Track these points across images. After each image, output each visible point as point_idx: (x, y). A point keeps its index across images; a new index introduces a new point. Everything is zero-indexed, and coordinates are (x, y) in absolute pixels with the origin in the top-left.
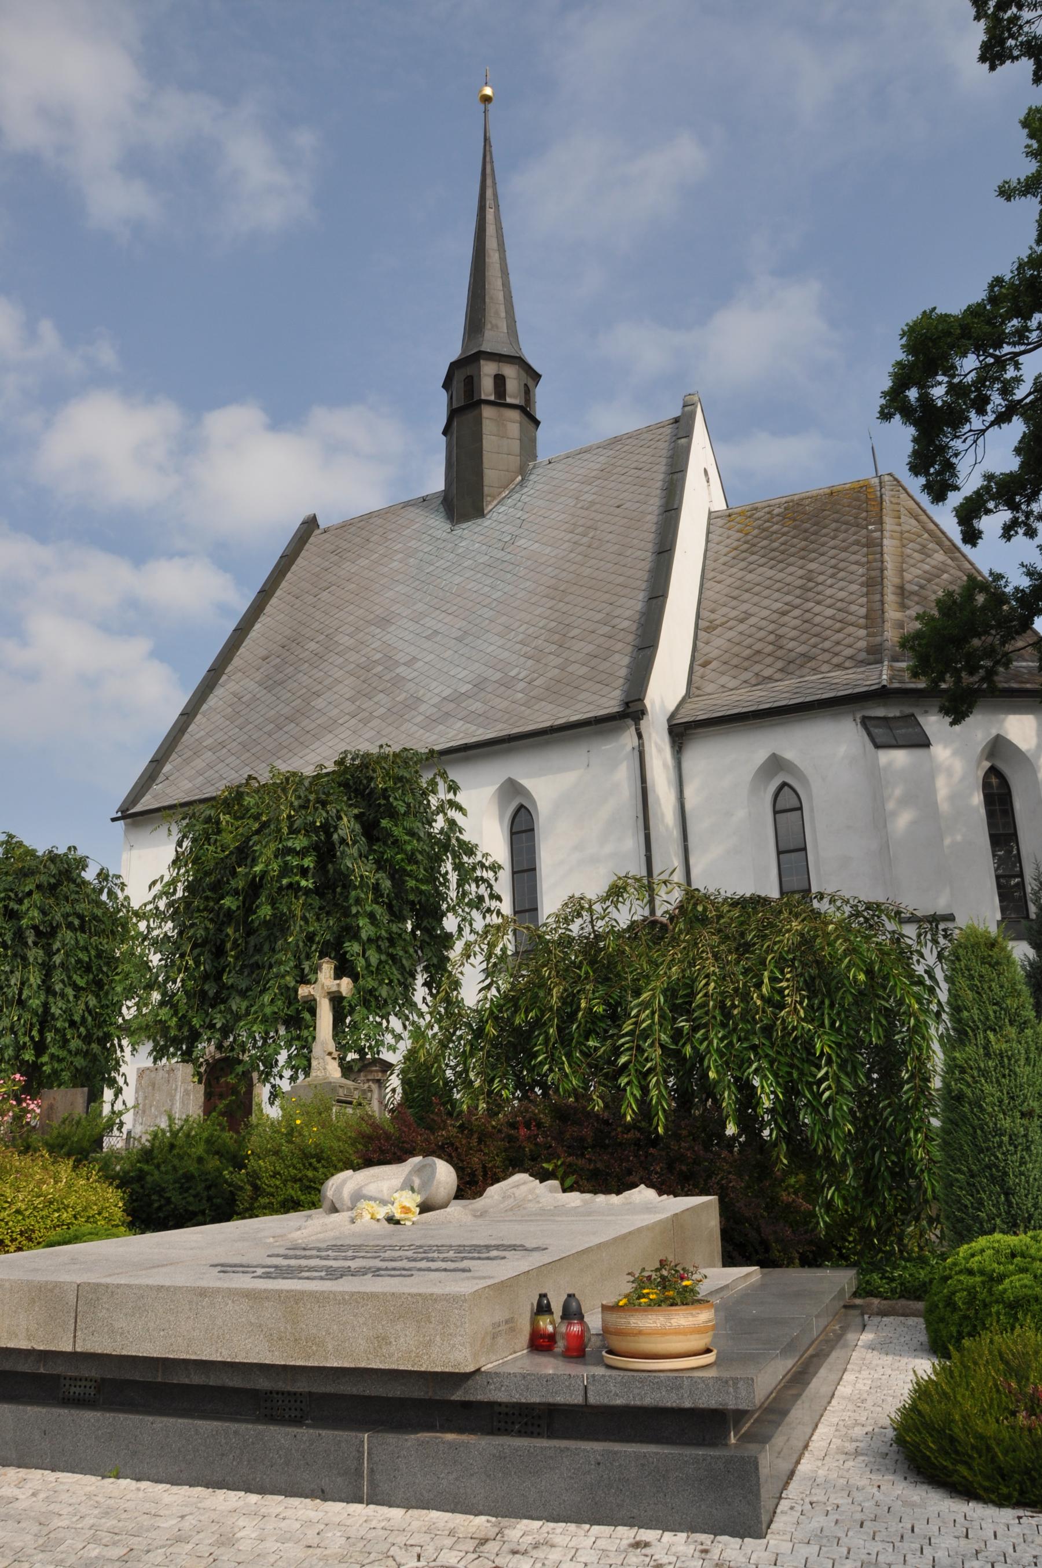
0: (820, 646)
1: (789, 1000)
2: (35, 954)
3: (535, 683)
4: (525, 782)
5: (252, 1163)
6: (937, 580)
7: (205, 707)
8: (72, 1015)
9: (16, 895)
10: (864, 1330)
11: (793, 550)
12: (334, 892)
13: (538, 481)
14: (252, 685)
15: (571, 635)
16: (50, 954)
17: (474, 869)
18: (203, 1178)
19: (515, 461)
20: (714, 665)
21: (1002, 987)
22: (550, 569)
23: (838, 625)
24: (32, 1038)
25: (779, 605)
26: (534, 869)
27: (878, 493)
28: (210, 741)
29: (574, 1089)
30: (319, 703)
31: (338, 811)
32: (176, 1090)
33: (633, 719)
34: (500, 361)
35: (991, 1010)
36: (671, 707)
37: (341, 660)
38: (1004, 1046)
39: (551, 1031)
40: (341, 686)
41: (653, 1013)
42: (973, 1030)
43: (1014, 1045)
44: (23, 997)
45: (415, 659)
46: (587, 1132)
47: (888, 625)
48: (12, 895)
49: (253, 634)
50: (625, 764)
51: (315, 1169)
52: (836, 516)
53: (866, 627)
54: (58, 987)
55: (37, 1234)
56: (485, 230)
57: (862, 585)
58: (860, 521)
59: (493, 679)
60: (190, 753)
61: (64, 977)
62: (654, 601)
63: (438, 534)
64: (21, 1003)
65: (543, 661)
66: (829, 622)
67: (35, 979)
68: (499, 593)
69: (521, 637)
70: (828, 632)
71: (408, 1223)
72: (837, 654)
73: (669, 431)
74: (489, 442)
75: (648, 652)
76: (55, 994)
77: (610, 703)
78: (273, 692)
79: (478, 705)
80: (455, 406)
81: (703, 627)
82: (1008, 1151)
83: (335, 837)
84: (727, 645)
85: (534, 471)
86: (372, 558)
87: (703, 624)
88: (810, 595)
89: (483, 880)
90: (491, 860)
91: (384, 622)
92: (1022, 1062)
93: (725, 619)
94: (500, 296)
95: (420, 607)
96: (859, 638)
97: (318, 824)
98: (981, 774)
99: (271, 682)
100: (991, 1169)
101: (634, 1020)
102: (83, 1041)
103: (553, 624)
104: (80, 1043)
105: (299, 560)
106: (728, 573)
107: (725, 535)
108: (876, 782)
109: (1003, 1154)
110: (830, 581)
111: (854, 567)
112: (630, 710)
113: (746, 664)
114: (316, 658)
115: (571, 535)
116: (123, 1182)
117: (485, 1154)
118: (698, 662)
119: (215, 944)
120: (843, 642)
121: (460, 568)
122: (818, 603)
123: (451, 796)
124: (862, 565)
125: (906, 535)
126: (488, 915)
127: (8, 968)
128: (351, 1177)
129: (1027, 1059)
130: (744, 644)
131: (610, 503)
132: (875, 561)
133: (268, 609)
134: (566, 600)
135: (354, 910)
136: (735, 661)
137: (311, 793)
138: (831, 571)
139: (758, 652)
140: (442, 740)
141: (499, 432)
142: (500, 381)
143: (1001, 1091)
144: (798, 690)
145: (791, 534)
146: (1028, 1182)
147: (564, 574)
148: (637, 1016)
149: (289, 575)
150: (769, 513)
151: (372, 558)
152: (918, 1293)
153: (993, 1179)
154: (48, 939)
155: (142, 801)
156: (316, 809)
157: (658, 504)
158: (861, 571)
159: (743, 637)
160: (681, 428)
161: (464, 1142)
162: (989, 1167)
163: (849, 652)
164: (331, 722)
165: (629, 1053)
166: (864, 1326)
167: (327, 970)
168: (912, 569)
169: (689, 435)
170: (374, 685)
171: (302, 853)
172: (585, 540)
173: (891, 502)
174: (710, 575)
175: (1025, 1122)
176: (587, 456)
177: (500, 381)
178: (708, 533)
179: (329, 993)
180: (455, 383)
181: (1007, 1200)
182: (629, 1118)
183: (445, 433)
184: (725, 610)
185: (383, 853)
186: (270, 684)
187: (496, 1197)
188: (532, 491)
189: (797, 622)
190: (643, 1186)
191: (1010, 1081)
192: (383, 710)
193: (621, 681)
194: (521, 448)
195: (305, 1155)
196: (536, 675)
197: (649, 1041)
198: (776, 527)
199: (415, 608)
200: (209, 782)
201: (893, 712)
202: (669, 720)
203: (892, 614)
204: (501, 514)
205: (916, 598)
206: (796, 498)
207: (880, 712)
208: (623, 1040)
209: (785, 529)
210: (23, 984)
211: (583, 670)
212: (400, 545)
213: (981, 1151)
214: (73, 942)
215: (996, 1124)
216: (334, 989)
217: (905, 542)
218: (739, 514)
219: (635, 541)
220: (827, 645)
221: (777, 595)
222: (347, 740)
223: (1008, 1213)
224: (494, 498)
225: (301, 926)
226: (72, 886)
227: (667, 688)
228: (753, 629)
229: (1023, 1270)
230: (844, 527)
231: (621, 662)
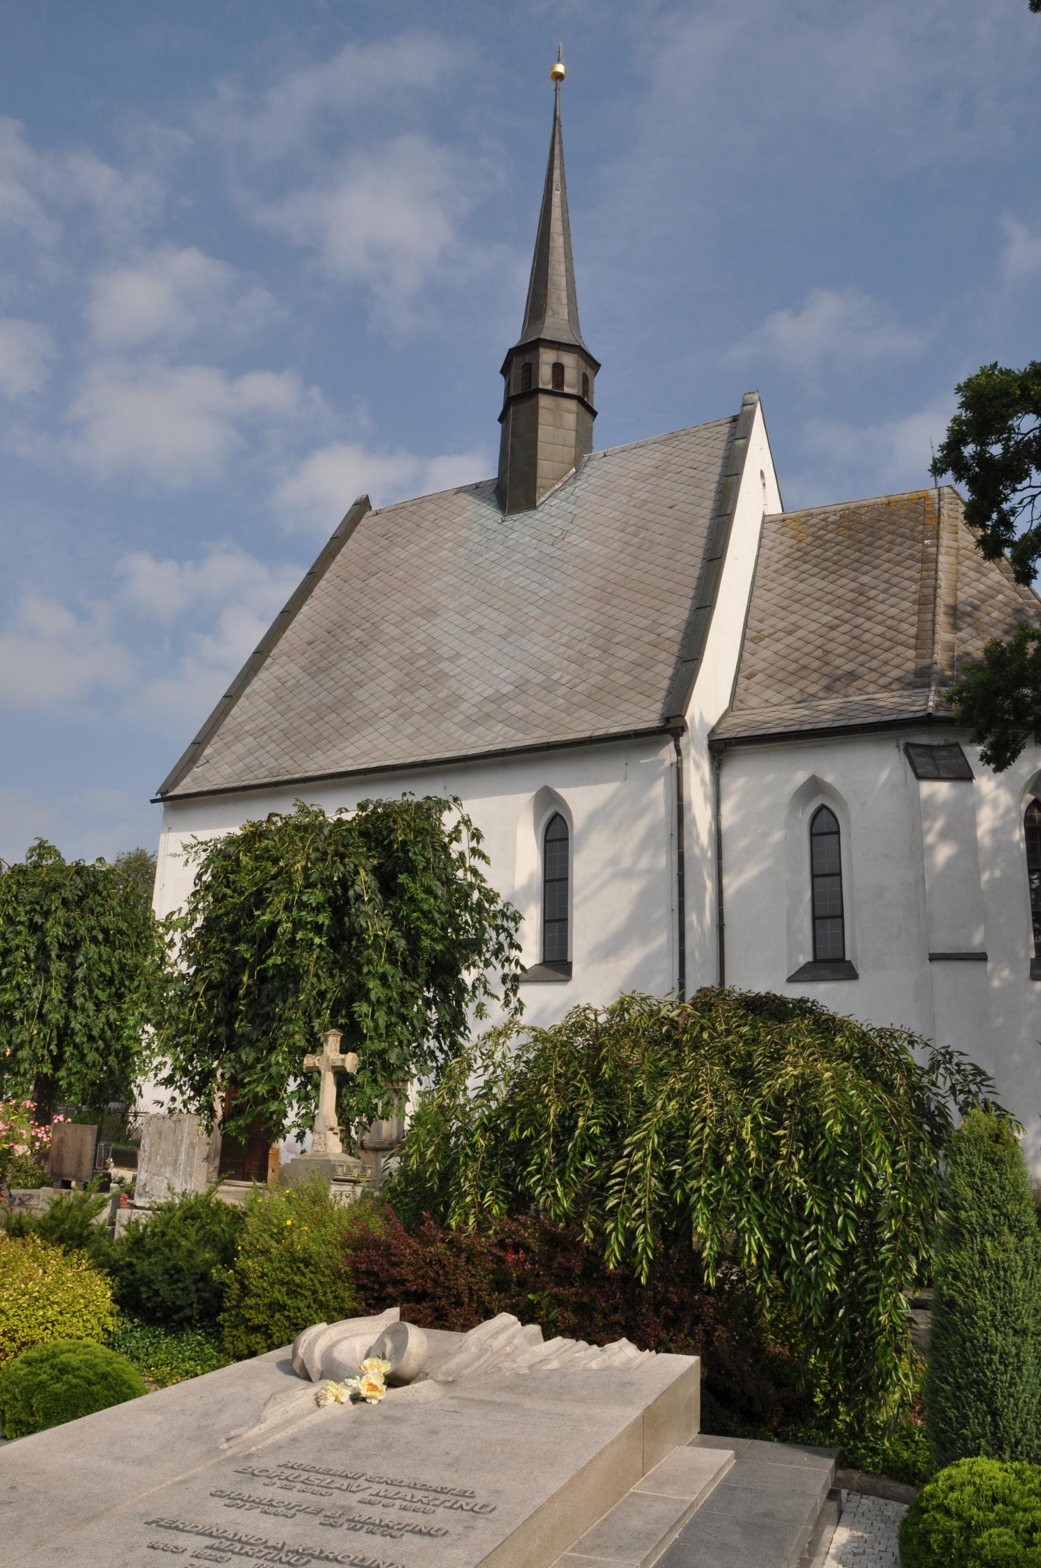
0: (867, 665)
1: (784, 1151)
2: (58, 967)
3: (576, 689)
4: (562, 792)
5: (241, 1262)
6: (991, 601)
7: (248, 690)
8: (90, 1030)
9: (42, 908)
10: (838, 1522)
11: (846, 561)
12: (350, 944)
13: (595, 471)
14: (296, 671)
15: (616, 640)
16: (73, 967)
17: (495, 917)
18: (192, 1271)
19: (570, 453)
20: (759, 677)
21: (1003, 1188)
22: (599, 569)
23: (887, 644)
24: (50, 1052)
25: (828, 618)
26: (566, 879)
27: (937, 506)
28: (251, 726)
29: (566, 1214)
30: (361, 694)
31: (355, 866)
32: (182, 1141)
33: (672, 735)
34: (559, 350)
35: (990, 1214)
36: (713, 720)
37: (386, 650)
38: (1001, 1256)
39: (546, 1151)
40: (384, 677)
41: (645, 1156)
42: (970, 1232)
43: (1012, 1256)
44: (44, 1011)
45: (458, 655)
46: (577, 1266)
47: (938, 647)
48: (38, 908)
49: (300, 617)
50: (662, 780)
51: (303, 1274)
52: (892, 527)
53: (916, 648)
54: (79, 1002)
55: (21, 1334)
56: (550, 213)
57: (914, 602)
58: (917, 534)
59: (536, 681)
60: (232, 737)
61: (86, 992)
62: (701, 611)
63: (489, 524)
64: (42, 1017)
65: (586, 666)
66: (878, 640)
67: (56, 994)
68: (547, 591)
69: (565, 639)
70: (877, 651)
71: (374, 1402)
72: (884, 675)
73: (727, 430)
74: (545, 432)
75: (690, 665)
76: (75, 1008)
77: (650, 717)
78: (317, 679)
79: (519, 708)
80: (513, 393)
81: (751, 637)
82: (998, 1369)
83: (351, 893)
84: (773, 658)
85: (589, 464)
86: (423, 545)
87: (750, 634)
88: (861, 610)
89: (505, 930)
90: (512, 909)
91: (430, 613)
92: (1018, 1276)
93: (773, 630)
94: (563, 281)
95: (466, 599)
96: (908, 661)
97: (336, 879)
98: (1024, 807)
99: (315, 668)
100: (979, 1385)
101: (626, 1159)
102: (101, 1055)
103: (598, 628)
104: (97, 1056)
105: (350, 542)
106: (779, 581)
107: (778, 541)
108: (919, 812)
109: (993, 1372)
110: (882, 597)
111: (907, 583)
112: (670, 726)
113: (792, 679)
114: (361, 646)
115: (622, 534)
116: (111, 1268)
117: (473, 1276)
118: (743, 673)
119: (229, 987)
120: (891, 663)
121: (509, 561)
122: (869, 619)
123: (474, 844)
124: (915, 581)
125: (962, 552)
126: (506, 964)
127: (30, 982)
128: (324, 1332)
129: (1025, 1270)
130: (790, 657)
131: (663, 503)
132: (929, 577)
133: (316, 591)
134: (614, 603)
135: (365, 970)
136: (781, 675)
137: (329, 844)
138: (884, 585)
139: (805, 667)
140: (481, 742)
141: (555, 424)
142: (558, 369)
143: (995, 1305)
144: (842, 711)
145: (845, 544)
146: (1016, 1405)
147: (613, 575)
148: (629, 1155)
149: (339, 557)
150: (824, 520)
151: (423, 545)
152: (901, 1474)
153: (980, 1397)
154: (72, 952)
155: (183, 783)
156: (334, 862)
157: (711, 507)
158: (914, 587)
159: (790, 651)
160: (739, 428)
161: (452, 1260)
162: (977, 1382)
163: (897, 673)
164: (372, 714)
165: (617, 1196)
166: (840, 1512)
167: (332, 1043)
168: (967, 588)
169: (746, 436)
170: (416, 679)
171: (318, 909)
172: (636, 540)
173: (949, 516)
174: (760, 582)
175: (1018, 1340)
176: (643, 451)
177: (558, 369)
178: (761, 537)
179: (333, 1067)
180: (513, 370)
181: (994, 1420)
182: (611, 1266)
183: (501, 419)
184: (773, 621)
185: (400, 909)
186: (315, 670)
187: (473, 1349)
188: (585, 485)
189: (846, 638)
190: (624, 1340)
191: (1004, 1295)
192: (423, 706)
193: (663, 693)
194: (577, 439)
195: (294, 1259)
196: (578, 681)
197: (640, 1186)
198: (830, 536)
199: (461, 600)
200: (249, 769)
201: (937, 741)
202: (709, 735)
203: (943, 635)
204: (552, 506)
205: (969, 620)
206: (852, 505)
207: (924, 740)
208: (613, 1181)
209: (840, 538)
210: (45, 997)
211: (627, 679)
212: (451, 533)
213: (969, 1364)
214: (96, 957)
215: (987, 1339)
216: (339, 1064)
217: (961, 559)
218: (794, 519)
219: (686, 546)
220: (874, 664)
221: (827, 608)
222: (387, 735)
223: (994, 1434)
224: (547, 489)
225: (312, 984)
226: (98, 898)
227: (709, 702)
228: (801, 643)
229: (1003, 1523)
230: (899, 540)
231: (664, 673)
